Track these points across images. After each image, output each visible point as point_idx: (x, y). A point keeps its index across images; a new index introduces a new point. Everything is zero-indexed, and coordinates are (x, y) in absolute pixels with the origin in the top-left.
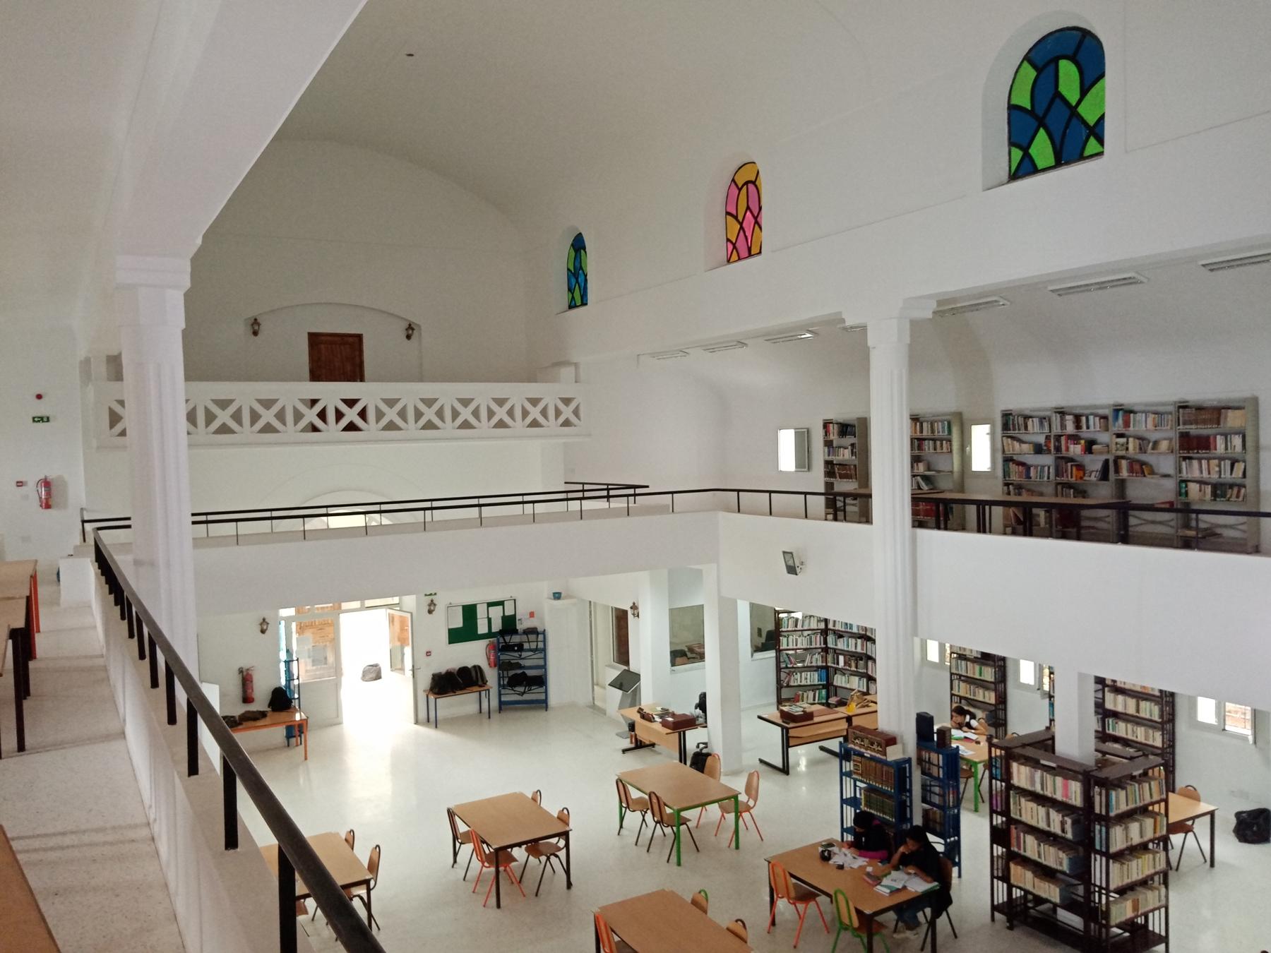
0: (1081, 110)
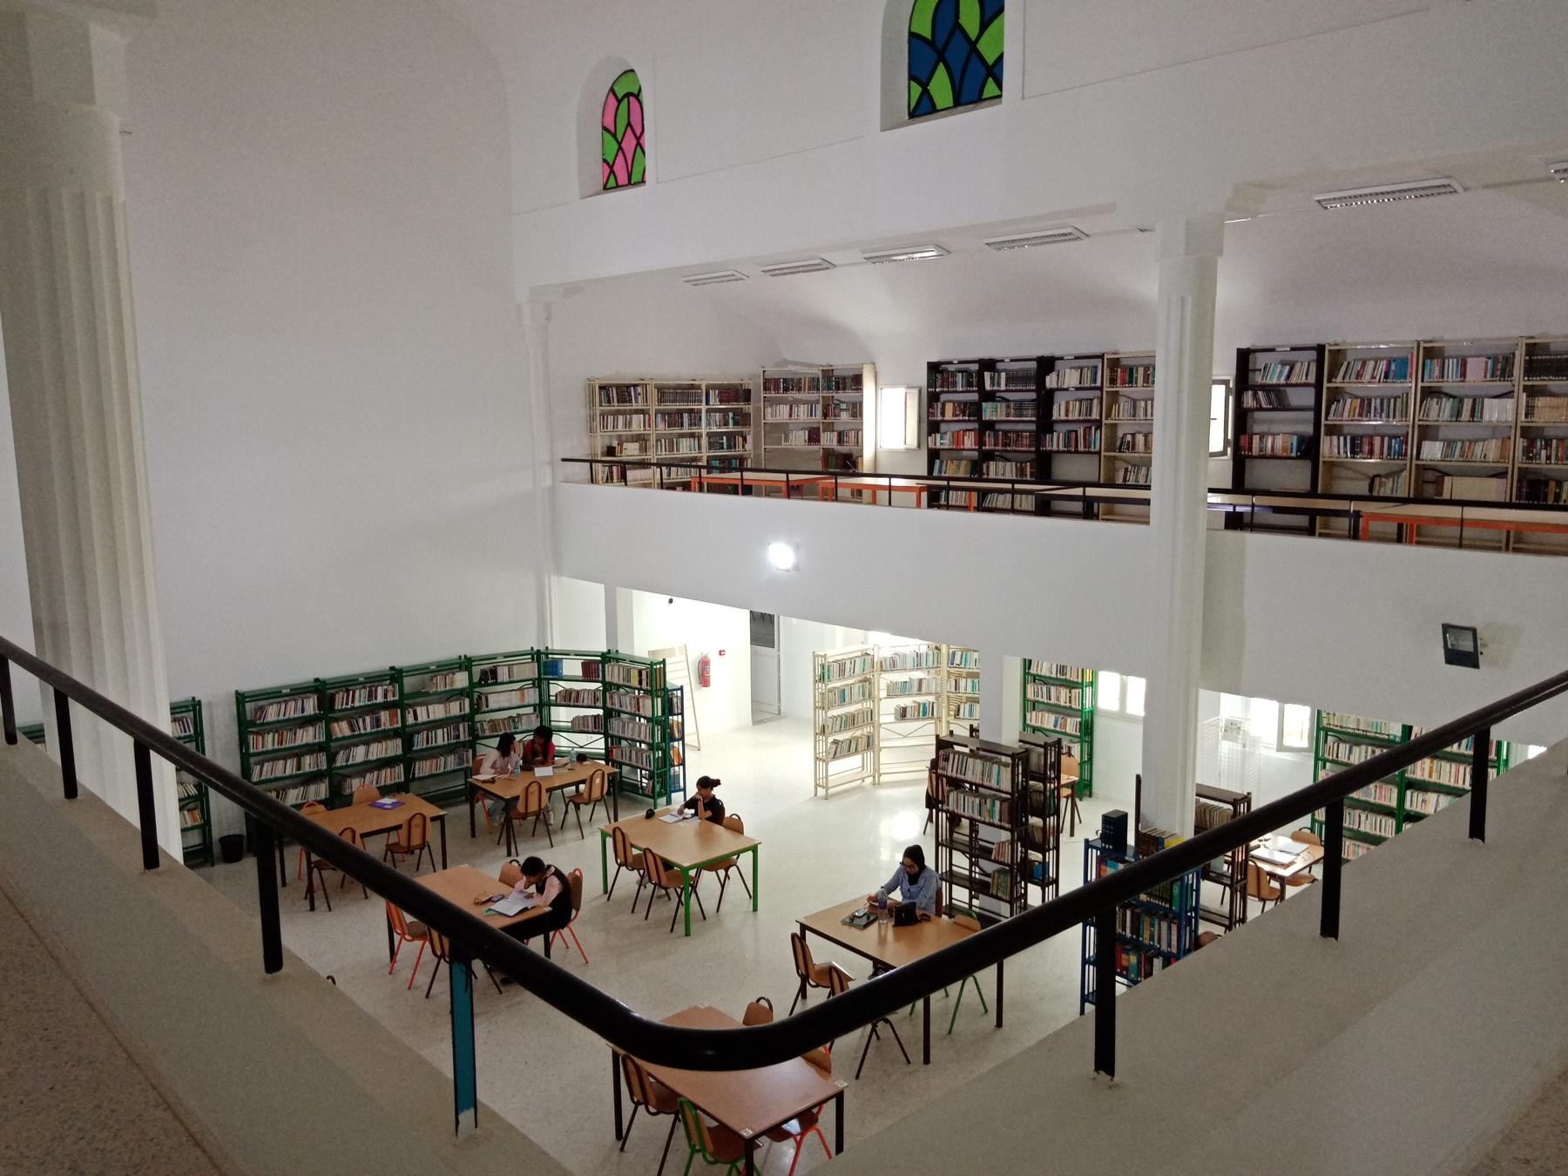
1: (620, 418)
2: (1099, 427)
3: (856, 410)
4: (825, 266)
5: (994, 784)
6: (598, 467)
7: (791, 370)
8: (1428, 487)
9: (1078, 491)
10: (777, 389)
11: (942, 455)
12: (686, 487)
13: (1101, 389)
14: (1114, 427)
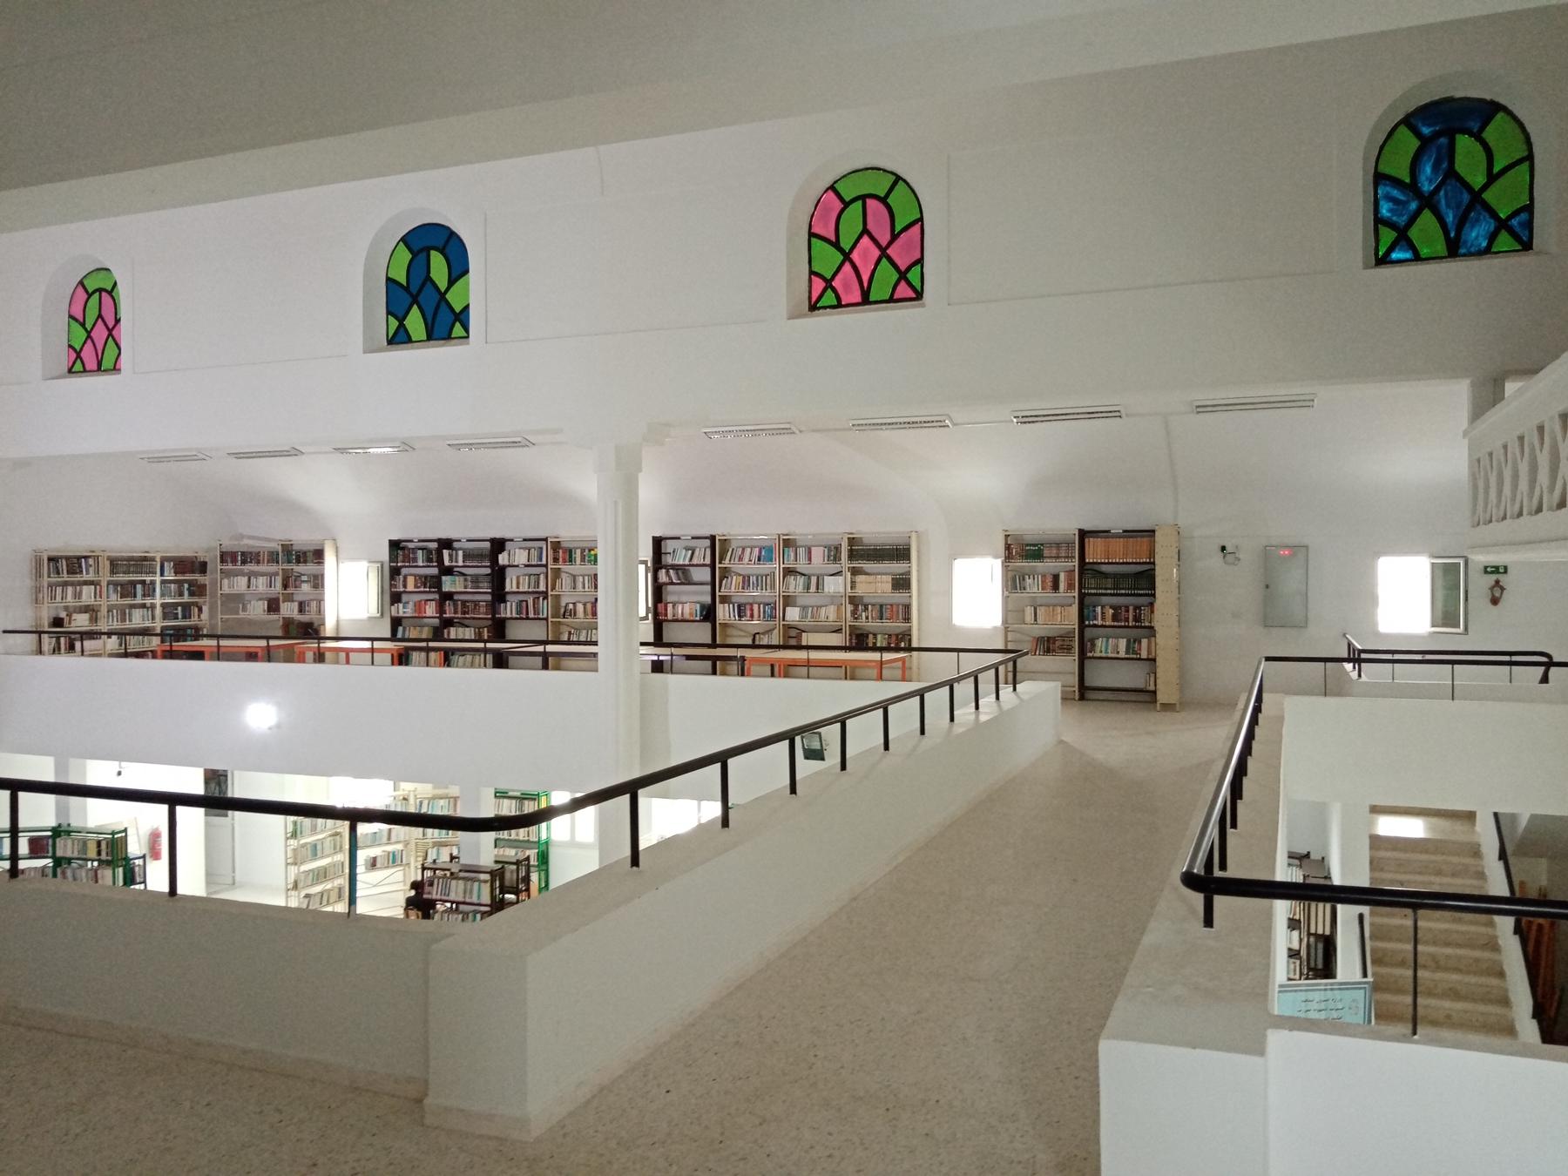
1: (70, 589)
2: (546, 598)
3: (318, 581)
4: (294, 452)
5: (475, 900)
6: (45, 637)
7: (247, 544)
8: (792, 639)
9: (540, 649)
10: (234, 561)
11: (405, 622)
12: (251, 656)
13: (546, 566)
14: (558, 597)
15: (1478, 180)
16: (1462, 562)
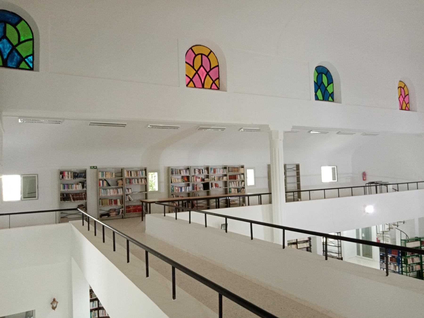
0: (328, 88)
15: (15, 42)
16: (36, 176)
